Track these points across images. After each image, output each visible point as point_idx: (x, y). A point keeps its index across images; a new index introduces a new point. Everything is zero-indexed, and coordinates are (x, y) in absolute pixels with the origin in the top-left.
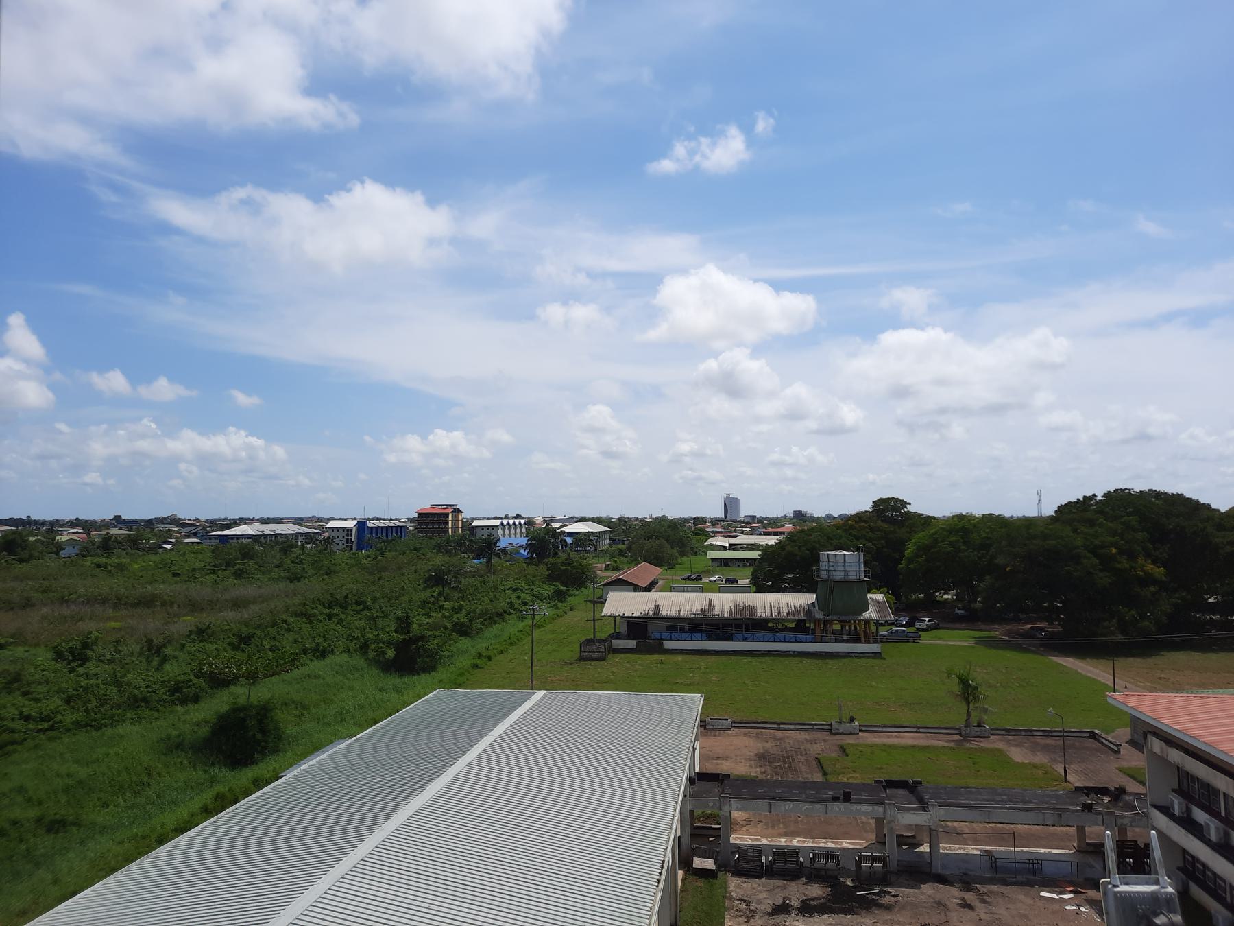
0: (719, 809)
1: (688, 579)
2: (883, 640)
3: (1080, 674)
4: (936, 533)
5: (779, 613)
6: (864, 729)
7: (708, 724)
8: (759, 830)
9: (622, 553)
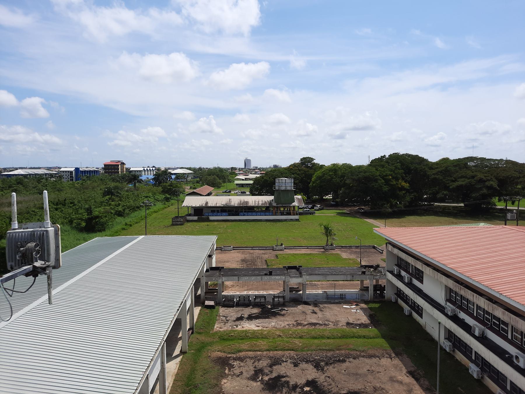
0: (217, 281)
1: (225, 192)
2: (300, 214)
3: (374, 225)
4: (324, 171)
5: (258, 204)
6: (286, 248)
7: (223, 248)
8: (236, 289)
9: (198, 182)
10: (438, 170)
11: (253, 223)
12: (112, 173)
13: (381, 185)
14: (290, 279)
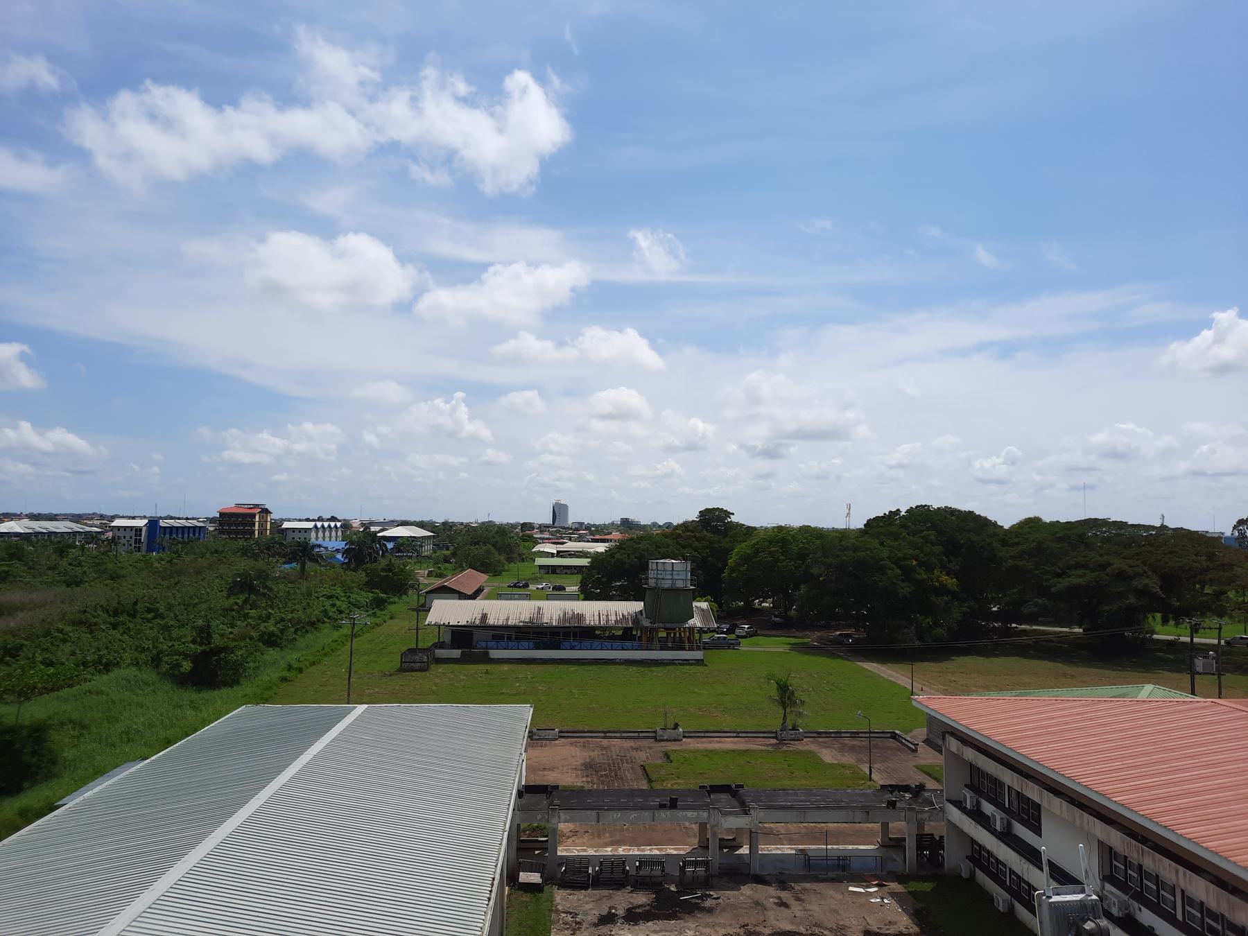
1: (515, 586)
2: (706, 647)
4: (758, 543)
9: (446, 560)
10: (1019, 548)
11: (595, 668)
12: (237, 533)
13: (895, 581)
14: (723, 819)
